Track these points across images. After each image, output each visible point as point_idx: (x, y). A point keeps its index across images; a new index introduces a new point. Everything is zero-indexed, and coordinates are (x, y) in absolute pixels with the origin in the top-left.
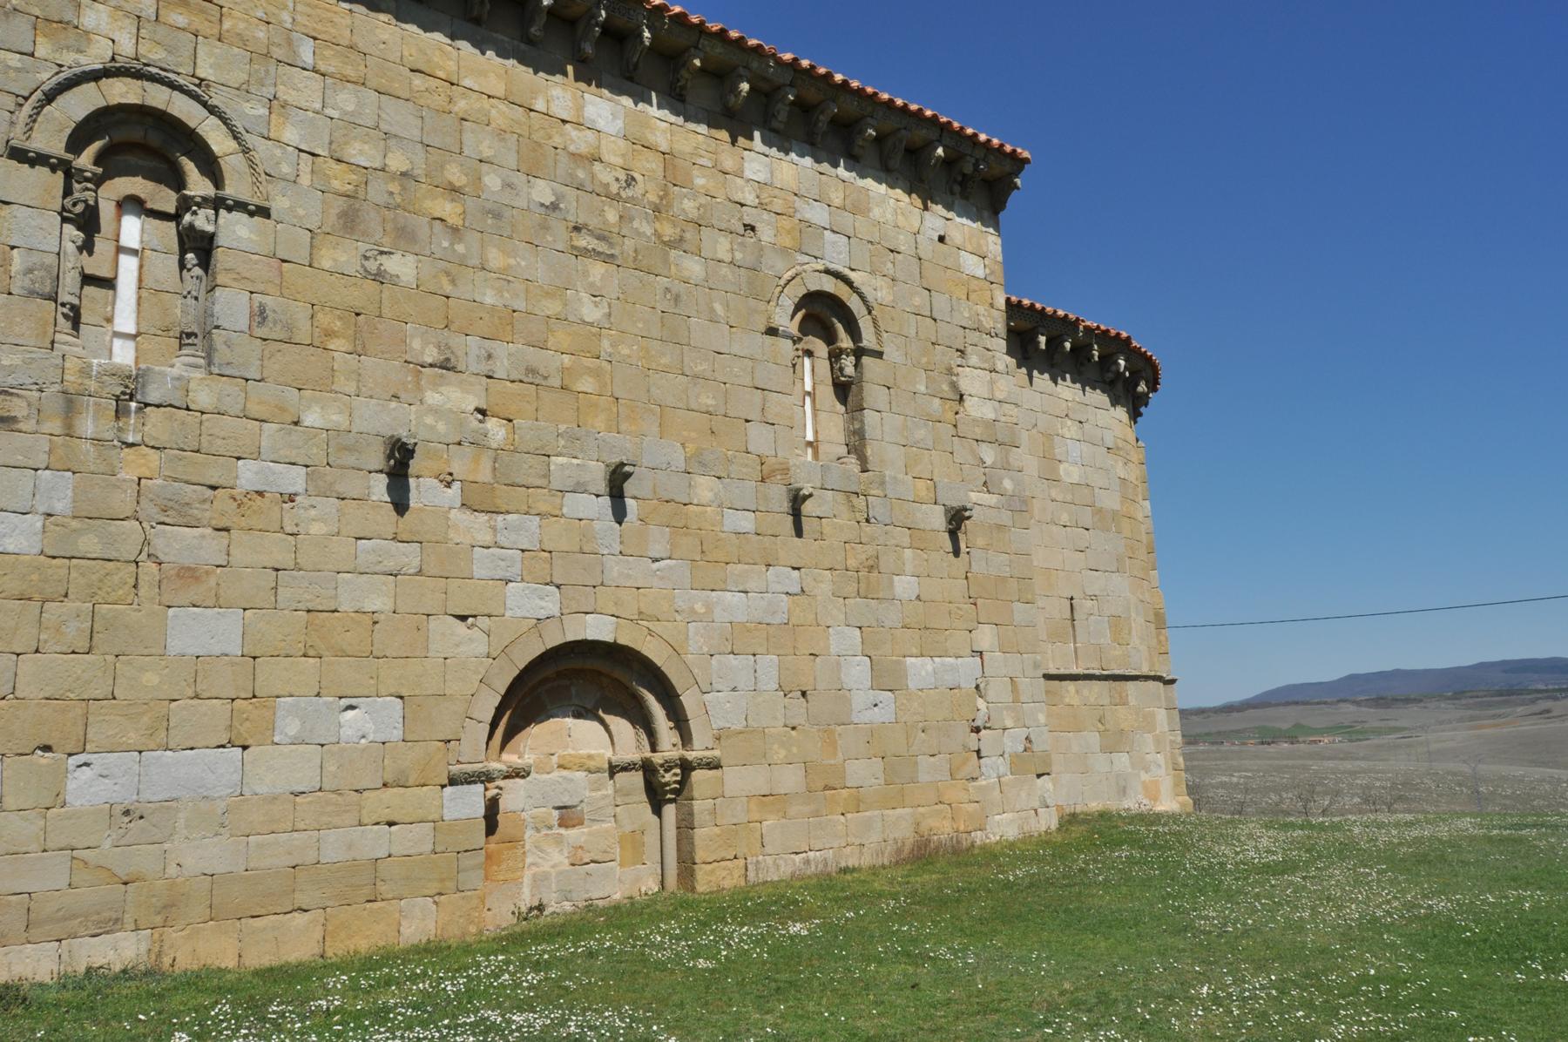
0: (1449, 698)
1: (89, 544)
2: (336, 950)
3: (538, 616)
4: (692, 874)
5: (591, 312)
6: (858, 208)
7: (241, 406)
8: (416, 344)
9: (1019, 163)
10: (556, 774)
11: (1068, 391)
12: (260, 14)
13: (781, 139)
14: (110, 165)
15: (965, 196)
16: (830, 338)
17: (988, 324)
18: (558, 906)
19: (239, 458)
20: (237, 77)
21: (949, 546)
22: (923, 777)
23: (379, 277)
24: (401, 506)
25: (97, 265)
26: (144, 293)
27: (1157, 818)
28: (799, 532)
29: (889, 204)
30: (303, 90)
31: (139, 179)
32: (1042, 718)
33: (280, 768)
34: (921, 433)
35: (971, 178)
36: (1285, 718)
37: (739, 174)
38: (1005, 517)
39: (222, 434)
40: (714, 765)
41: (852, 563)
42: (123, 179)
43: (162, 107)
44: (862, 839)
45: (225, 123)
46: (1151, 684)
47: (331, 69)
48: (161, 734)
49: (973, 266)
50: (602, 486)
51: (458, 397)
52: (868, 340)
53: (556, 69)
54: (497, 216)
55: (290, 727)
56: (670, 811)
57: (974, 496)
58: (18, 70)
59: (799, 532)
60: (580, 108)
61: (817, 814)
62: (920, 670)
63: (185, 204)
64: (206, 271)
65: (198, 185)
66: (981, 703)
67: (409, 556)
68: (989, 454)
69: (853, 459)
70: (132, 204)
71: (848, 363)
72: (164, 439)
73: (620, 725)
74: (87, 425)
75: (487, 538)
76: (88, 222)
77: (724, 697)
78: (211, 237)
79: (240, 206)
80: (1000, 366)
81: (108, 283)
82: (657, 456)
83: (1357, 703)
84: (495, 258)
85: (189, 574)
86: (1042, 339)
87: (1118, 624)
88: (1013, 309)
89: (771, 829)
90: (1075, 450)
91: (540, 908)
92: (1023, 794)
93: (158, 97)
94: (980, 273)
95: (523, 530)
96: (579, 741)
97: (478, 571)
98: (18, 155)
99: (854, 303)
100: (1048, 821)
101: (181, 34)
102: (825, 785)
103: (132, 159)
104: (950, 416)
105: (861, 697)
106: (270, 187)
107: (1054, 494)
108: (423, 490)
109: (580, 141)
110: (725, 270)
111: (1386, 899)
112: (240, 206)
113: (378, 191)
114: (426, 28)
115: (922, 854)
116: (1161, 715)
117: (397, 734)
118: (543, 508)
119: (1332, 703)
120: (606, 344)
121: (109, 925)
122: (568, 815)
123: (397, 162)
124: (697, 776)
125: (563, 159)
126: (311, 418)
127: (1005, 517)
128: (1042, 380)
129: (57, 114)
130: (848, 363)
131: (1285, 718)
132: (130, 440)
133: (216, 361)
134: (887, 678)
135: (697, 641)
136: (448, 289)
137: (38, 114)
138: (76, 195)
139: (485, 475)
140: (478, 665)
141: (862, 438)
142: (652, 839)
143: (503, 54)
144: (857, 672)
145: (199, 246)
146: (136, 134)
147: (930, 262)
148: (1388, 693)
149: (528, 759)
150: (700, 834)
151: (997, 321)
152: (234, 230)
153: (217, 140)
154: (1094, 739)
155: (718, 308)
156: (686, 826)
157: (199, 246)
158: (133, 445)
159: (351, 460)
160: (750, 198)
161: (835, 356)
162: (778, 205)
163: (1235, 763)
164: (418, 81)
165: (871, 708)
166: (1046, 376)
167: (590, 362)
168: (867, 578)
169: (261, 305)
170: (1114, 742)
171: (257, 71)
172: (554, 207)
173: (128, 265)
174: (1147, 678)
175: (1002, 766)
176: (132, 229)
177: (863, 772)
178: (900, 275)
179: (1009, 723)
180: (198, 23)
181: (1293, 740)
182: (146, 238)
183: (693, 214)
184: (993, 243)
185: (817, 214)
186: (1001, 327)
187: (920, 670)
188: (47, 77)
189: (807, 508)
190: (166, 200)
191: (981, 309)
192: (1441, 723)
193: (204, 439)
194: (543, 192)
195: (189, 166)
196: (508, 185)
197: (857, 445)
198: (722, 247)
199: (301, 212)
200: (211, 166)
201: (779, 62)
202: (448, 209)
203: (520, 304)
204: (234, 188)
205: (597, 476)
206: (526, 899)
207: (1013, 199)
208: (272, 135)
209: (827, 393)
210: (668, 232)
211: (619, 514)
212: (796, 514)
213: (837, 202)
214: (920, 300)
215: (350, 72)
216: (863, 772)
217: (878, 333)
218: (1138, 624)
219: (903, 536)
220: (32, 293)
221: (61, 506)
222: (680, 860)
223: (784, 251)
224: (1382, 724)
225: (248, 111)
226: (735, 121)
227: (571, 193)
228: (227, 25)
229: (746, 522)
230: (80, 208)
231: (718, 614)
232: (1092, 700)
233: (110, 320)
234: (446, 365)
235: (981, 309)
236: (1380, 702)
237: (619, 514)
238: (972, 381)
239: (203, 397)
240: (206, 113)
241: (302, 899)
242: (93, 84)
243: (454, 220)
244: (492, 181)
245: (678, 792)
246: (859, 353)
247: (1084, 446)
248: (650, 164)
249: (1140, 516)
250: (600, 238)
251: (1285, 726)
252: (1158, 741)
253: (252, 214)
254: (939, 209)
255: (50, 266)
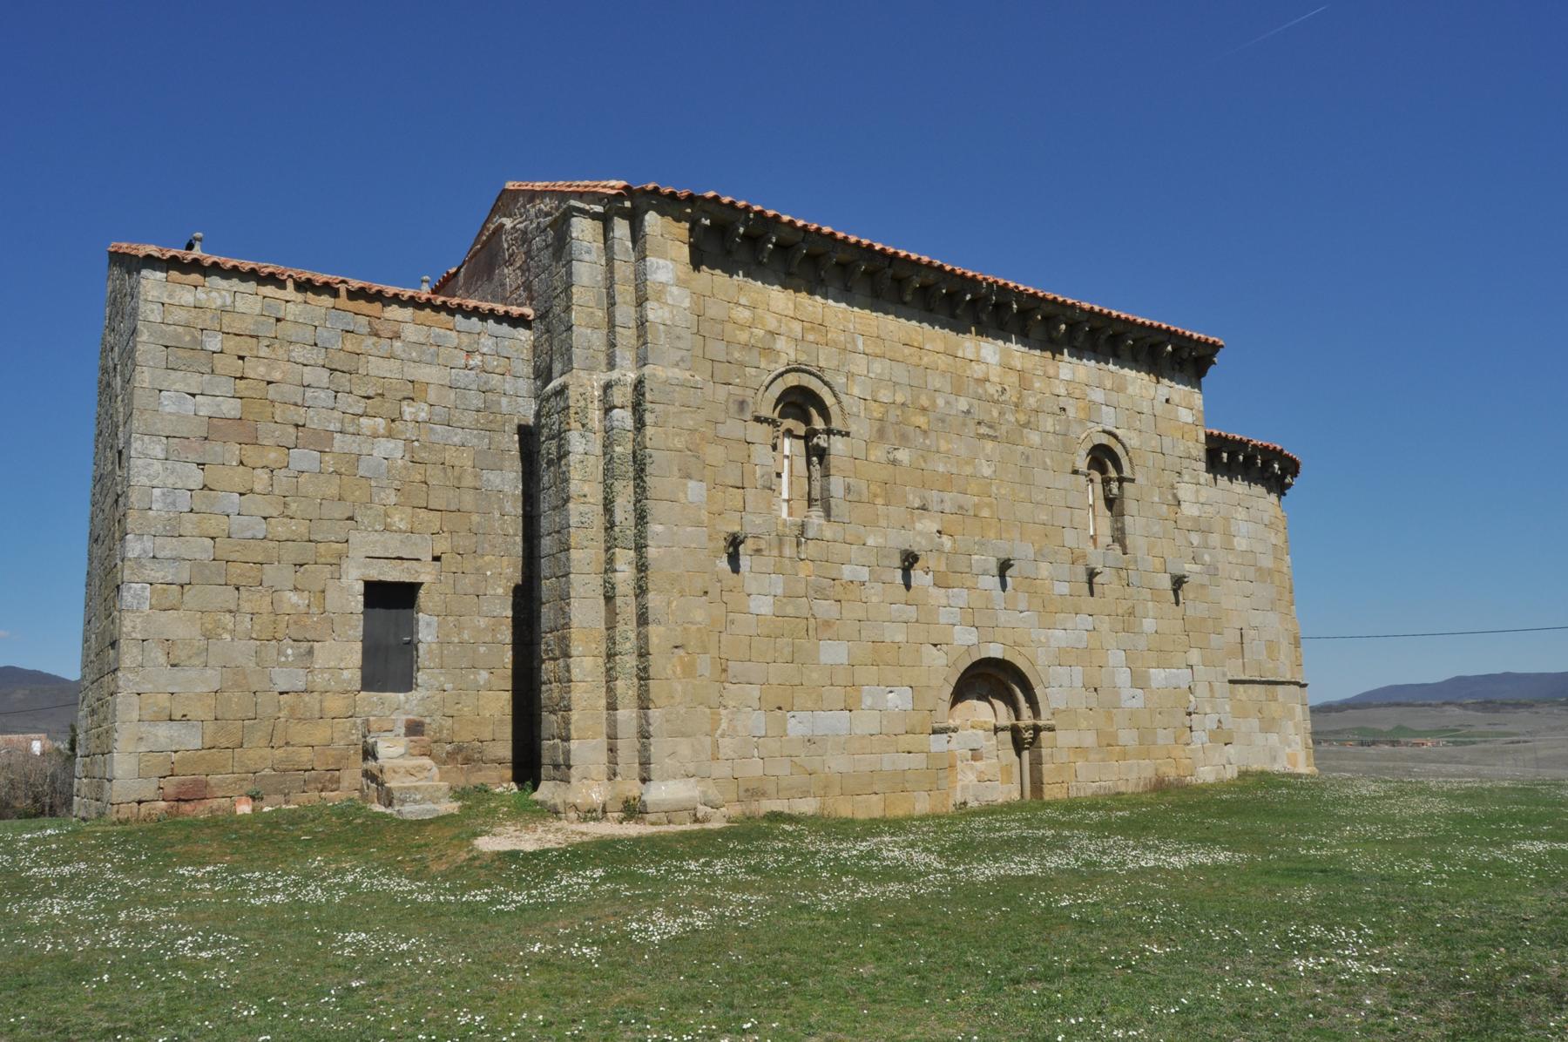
0: (1561, 704)
1: (790, 610)
2: (891, 814)
3: (969, 644)
4: (1041, 790)
5: (987, 471)
6: (1120, 388)
8: (911, 497)
9: (1215, 348)
10: (971, 731)
11: (1240, 487)
13: (1078, 353)
15: (1181, 371)
16: (1103, 471)
17: (1194, 453)
18: (973, 804)
20: (834, 364)
21: (1173, 599)
22: (1160, 742)
23: (894, 462)
24: (908, 586)
27: (1300, 776)
28: (1092, 594)
29: (1137, 382)
30: (859, 365)
32: (1228, 708)
33: (866, 722)
34: (1156, 528)
35: (1184, 359)
36: (1386, 720)
37: (1057, 377)
38: (1205, 579)
40: (1051, 729)
41: (1120, 611)
44: (1128, 775)
46: (1292, 687)
48: (820, 705)
49: (1186, 416)
50: (995, 571)
51: (929, 525)
52: (1127, 473)
53: (966, 331)
54: (943, 421)
55: (868, 701)
56: (1026, 754)
57: (1187, 566)
59: (1092, 594)
60: (978, 352)
61: (1103, 760)
62: (1158, 676)
63: (815, 433)
65: (818, 423)
66: (1192, 698)
67: (911, 613)
68: (1195, 538)
69: (1117, 546)
71: (1114, 486)
73: (999, 705)
75: (944, 601)
77: (1057, 690)
78: (824, 449)
79: (839, 433)
80: (1202, 481)
82: (1021, 551)
83: (1464, 706)
84: (944, 446)
85: (827, 624)
86: (1225, 455)
87: (1271, 646)
88: (1209, 437)
89: (1080, 766)
90: (1244, 528)
91: (965, 803)
94: (1190, 420)
95: (961, 596)
96: (983, 712)
97: (942, 620)
99: (1118, 449)
100: (1231, 773)
102: (1108, 743)
104: (1172, 516)
105: (1126, 692)
107: (1230, 558)
108: (917, 575)
109: (978, 370)
110: (1051, 438)
111: (1440, 806)
112: (839, 433)
113: (894, 414)
114: (909, 319)
115: (1160, 786)
116: (1298, 708)
117: (910, 707)
118: (969, 584)
119: (1436, 706)
120: (994, 488)
121: (805, 794)
122: (976, 754)
123: (900, 399)
124: (1043, 734)
125: (972, 383)
126: (870, 542)
127: (1205, 579)
128: (1223, 481)
130: (1114, 486)
131: (1386, 720)
135: (1042, 658)
136: (923, 465)
139: (943, 568)
140: (943, 669)
141: (1123, 533)
142: (1016, 770)
143: (942, 327)
144: (1123, 677)
147: (1157, 415)
148: (1495, 697)
149: (958, 722)
150: (1046, 767)
151: (1199, 450)
153: (829, 400)
154: (1255, 723)
156: (1036, 763)
159: (886, 562)
160: (1062, 392)
161: (1106, 482)
162: (1077, 394)
163: (1334, 763)
164: (907, 350)
165: (1132, 699)
167: (987, 500)
170: (1268, 725)
172: (968, 412)
174: (1290, 683)
175: (1204, 737)
177: (1127, 737)
178: (1143, 428)
181: (1394, 743)
183: (1034, 406)
184: (1197, 398)
185: (1098, 396)
186: (1202, 455)
187: (1158, 676)
189: (1097, 579)
190: (801, 429)
191: (1190, 444)
192: (1554, 729)
194: (963, 404)
195: (813, 412)
196: (947, 403)
197: (1119, 537)
198: (1049, 423)
200: (825, 413)
201: (1082, 309)
202: (921, 420)
203: (954, 471)
204: (836, 424)
205: (993, 566)
206: (959, 799)
207: (1211, 370)
209: (1101, 504)
210: (1023, 418)
211: (1004, 586)
212: (1090, 583)
213: (1109, 386)
214: (1155, 443)
215: (878, 351)
216: (1127, 737)
217: (1132, 468)
218: (1285, 646)
219: (1146, 594)
221: (779, 591)
222: (1032, 782)
223: (1081, 422)
224: (1489, 729)
225: (839, 381)
226: (1052, 345)
227: (976, 402)
229: (1064, 588)
231: (1053, 643)
234: (923, 508)
235: (1190, 444)
236: (1487, 705)
237: (1004, 586)
238: (1185, 491)
239: (828, 534)
241: (876, 788)
243: (924, 427)
244: (940, 402)
245: (1031, 744)
246: (1121, 480)
247: (1251, 525)
248: (1013, 379)
249: (1285, 570)
250: (991, 427)
251: (1386, 728)
252: (1296, 726)
254: (1166, 381)
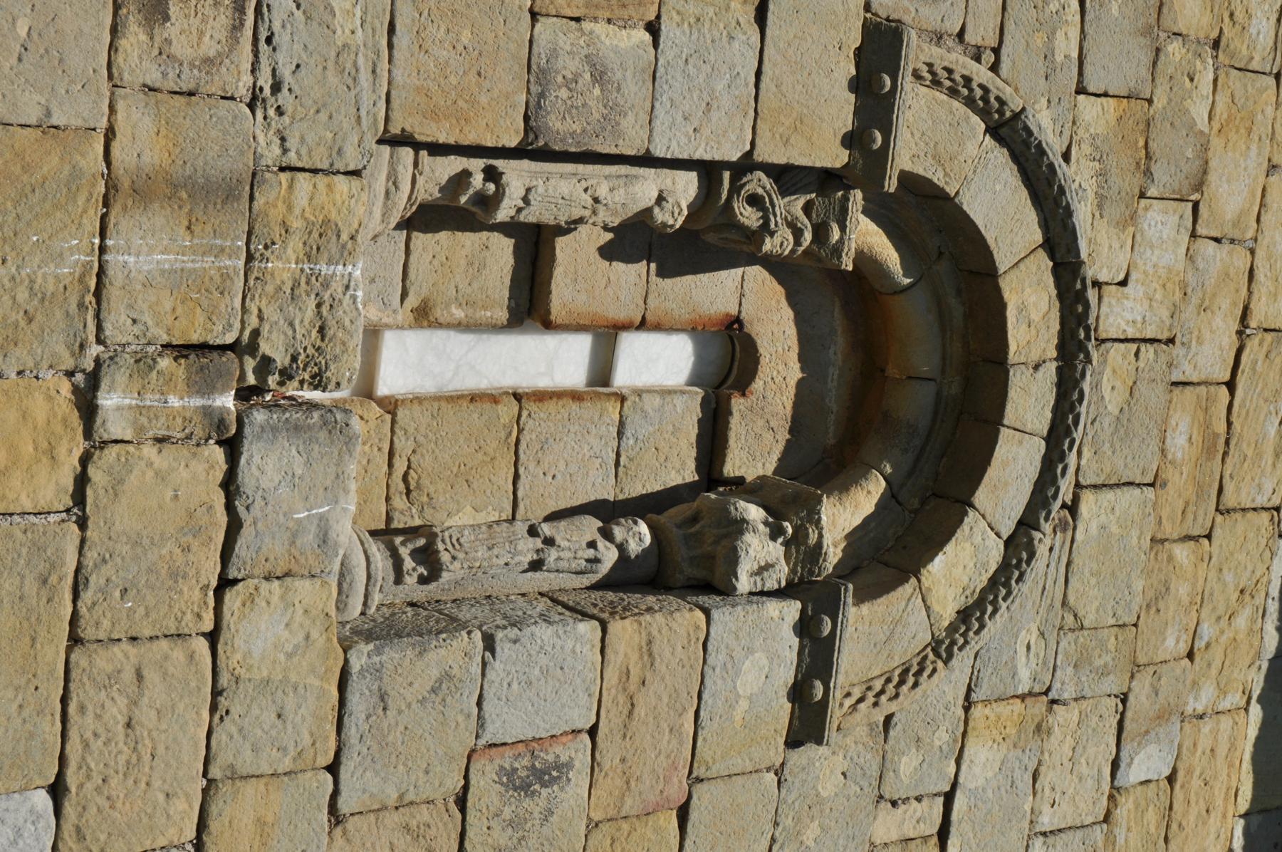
7: (246, 762)
12: (1207, 631)
14: (827, 289)
19: (57, 790)
20: (1091, 599)
25: (578, 272)
26: (508, 410)
31: (795, 373)
39: (146, 716)
42: (792, 331)
43: (1010, 416)
45: (993, 582)
47: (1120, 834)
58: (1048, 56)
64: (603, 585)
70: (728, 360)
72: (116, 514)
74: (149, 252)
76: (701, 242)
78: (725, 590)
79: (817, 655)
81: (529, 306)
93: (1029, 401)
98: (880, 48)
101: (1154, 446)
103: (837, 350)
106: (861, 732)
112: (817, 655)
129: (971, 149)
132: (108, 400)
133: (392, 655)
137: (970, 102)
138: (780, 202)
145: (677, 553)
146: (919, 346)
152: (755, 646)
157: (677, 553)
158: (87, 407)
169: (563, 768)
171: (1102, 645)
173: (559, 359)
176: (660, 363)
180: (1178, 481)
182: (651, 403)
188: (1045, 125)
190: (755, 450)
193: (124, 655)
199: (811, 833)
200: (890, 555)
208: (977, 712)
220: (537, 74)
225: (1017, 638)
228: (1182, 553)
230: (749, 216)
233: (424, 316)
240: (1007, 529)
242: (1038, 237)
253: (798, 693)
255: (617, 133)
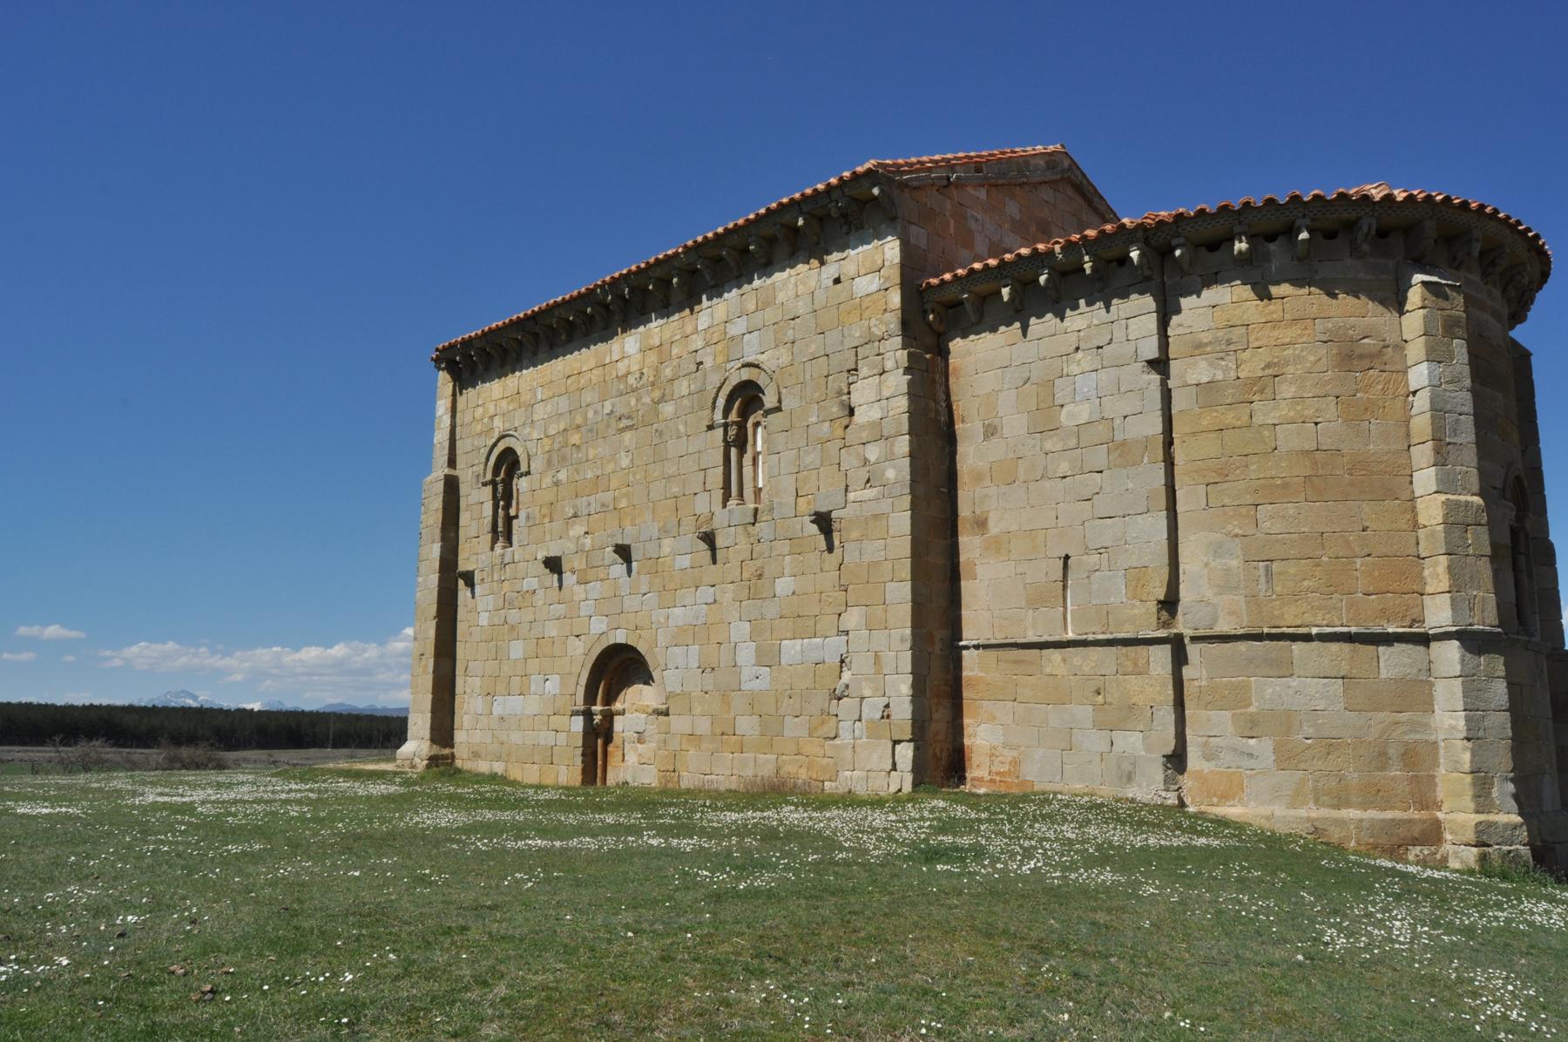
13: (716, 290)
15: (860, 227)
21: (823, 545)
28: (714, 562)
59: (714, 562)
62: (792, 649)
92: (875, 757)
102: (725, 734)
104: (839, 432)
107: (1048, 446)
128: (1043, 325)
134: (769, 658)
144: (746, 654)
155: (682, 428)
165: (755, 679)
166: (1049, 316)
168: (756, 584)
177: (747, 725)
179: (867, 693)
187: (792, 649)
216: (747, 725)
226: (690, 300)
232: (1086, 669)
